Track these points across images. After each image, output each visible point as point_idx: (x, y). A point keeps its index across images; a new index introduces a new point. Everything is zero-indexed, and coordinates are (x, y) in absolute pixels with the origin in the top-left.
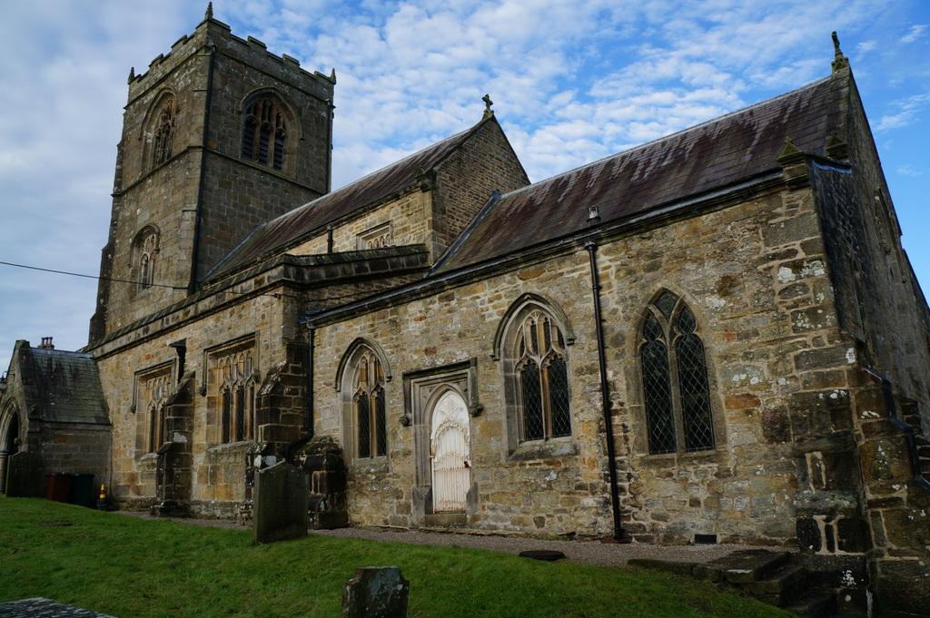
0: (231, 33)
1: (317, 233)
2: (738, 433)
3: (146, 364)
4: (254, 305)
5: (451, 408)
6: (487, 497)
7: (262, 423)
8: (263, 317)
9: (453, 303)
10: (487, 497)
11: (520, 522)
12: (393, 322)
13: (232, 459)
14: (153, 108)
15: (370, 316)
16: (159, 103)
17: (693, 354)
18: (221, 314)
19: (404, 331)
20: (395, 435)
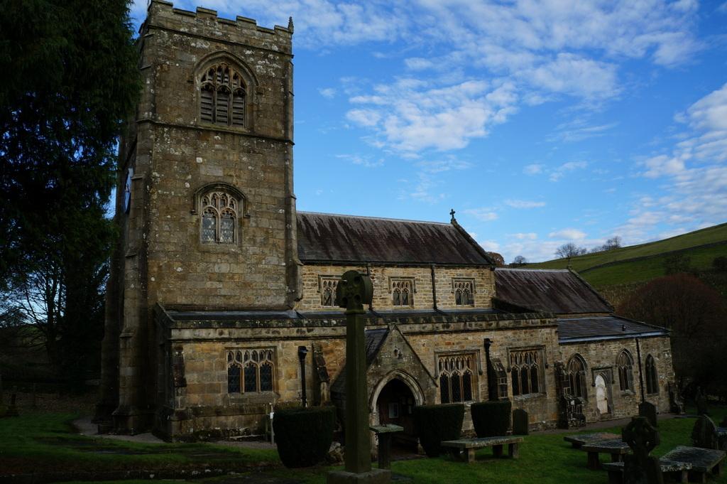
0: (257, 25)
2: (662, 389)
3: (444, 348)
5: (600, 381)
10: (616, 408)
12: (585, 349)
13: (533, 403)
14: (208, 59)
16: (214, 59)
17: (653, 369)
18: (518, 331)
20: (589, 390)
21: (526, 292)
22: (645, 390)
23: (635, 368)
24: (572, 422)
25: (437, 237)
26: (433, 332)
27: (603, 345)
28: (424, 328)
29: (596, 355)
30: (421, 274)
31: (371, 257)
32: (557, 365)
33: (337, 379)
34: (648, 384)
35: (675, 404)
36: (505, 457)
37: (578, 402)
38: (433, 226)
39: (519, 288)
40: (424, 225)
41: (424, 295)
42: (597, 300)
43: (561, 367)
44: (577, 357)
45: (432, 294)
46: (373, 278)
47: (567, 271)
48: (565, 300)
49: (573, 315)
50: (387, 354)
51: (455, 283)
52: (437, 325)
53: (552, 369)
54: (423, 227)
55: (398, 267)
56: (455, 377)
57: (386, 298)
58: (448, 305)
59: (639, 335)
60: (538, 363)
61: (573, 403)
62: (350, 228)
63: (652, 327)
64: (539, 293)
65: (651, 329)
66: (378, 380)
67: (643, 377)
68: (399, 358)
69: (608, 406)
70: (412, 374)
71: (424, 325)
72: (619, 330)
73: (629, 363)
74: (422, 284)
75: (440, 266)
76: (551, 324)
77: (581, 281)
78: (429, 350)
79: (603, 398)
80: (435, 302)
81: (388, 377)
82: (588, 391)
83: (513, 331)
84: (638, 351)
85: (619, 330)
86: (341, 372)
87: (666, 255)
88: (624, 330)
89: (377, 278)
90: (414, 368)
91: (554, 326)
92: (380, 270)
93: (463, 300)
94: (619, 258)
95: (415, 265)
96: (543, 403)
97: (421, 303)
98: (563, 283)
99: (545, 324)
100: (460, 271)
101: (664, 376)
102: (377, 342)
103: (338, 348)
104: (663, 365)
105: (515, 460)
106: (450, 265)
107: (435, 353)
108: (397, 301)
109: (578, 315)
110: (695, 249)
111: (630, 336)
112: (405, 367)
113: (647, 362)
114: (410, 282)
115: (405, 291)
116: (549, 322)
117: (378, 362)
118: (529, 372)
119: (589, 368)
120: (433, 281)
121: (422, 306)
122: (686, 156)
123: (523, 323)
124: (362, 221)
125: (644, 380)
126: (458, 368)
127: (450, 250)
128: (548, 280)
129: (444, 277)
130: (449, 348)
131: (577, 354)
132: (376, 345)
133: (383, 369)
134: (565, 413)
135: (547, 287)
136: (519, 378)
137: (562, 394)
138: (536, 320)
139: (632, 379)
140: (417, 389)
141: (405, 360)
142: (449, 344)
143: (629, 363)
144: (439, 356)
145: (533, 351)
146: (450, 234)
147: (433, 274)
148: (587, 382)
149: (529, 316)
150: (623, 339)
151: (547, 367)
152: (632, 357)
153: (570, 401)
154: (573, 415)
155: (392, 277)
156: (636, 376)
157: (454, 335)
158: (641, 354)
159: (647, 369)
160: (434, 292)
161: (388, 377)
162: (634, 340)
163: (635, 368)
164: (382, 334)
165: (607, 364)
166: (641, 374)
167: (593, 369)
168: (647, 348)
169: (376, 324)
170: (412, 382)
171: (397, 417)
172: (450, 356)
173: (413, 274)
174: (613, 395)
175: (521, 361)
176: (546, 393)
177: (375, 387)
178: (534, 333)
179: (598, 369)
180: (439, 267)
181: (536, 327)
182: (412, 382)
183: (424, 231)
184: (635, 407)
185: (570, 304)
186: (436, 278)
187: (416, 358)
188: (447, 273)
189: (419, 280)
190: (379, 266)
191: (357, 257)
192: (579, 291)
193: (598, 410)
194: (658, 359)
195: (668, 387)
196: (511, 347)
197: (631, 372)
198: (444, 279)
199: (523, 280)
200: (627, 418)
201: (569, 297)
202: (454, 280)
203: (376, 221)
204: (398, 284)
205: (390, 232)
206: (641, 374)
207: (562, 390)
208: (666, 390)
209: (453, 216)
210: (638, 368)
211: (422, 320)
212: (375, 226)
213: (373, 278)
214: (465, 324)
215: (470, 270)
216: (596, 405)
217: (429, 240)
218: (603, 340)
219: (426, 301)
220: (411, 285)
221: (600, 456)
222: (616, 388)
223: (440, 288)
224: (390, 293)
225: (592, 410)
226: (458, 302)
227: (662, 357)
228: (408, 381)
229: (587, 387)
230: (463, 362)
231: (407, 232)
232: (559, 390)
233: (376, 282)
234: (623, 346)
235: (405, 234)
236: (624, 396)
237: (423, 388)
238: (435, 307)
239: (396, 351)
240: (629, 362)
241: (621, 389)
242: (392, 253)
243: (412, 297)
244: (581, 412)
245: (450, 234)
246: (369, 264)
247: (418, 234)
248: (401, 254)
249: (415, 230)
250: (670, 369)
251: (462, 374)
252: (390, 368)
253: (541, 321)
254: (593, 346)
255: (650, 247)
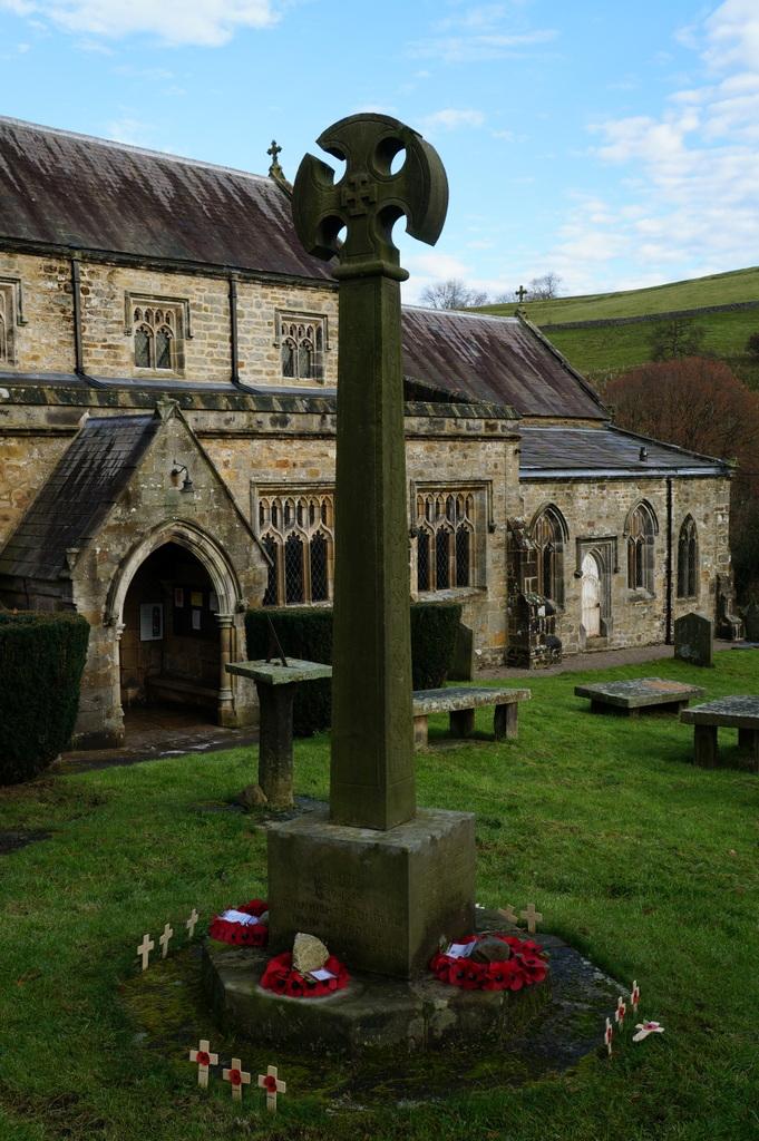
1: (210, 273)
2: (704, 590)
4: (484, 449)
5: (589, 566)
6: (617, 626)
7: (528, 576)
8: (496, 466)
9: (605, 492)
10: (617, 626)
11: (630, 639)
15: (555, 485)
17: (693, 545)
18: (436, 444)
19: (576, 505)
21: (433, 360)
22: (674, 590)
23: (660, 541)
24: (538, 652)
25: (239, 206)
26: (249, 434)
27: (603, 488)
28: (227, 422)
29: (589, 509)
30: (205, 292)
31: (79, 235)
32: (513, 527)
33: (11, 541)
34: (680, 575)
35: (726, 620)
36: (480, 737)
37: (549, 611)
38: (229, 178)
39: (416, 350)
40: (206, 171)
41: (210, 345)
42: (579, 391)
43: (521, 531)
44: (552, 511)
45: (228, 344)
46: (86, 292)
47: (515, 321)
48: (513, 384)
49: (531, 420)
50: (153, 479)
51: (281, 323)
52: (259, 416)
53: (501, 535)
54: (204, 176)
55: (150, 268)
56: (294, 545)
57: (116, 347)
58: (264, 376)
59: (672, 472)
60: (472, 519)
61: (542, 611)
62: (20, 153)
63: (696, 457)
64: (459, 365)
65: (693, 462)
66: (129, 545)
67: (673, 562)
68: (182, 491)
69: (601, 621)
70: (213, 533)
71: (229, 415)
72: (634, 459)
73: (648, 530)
74: (206, 318)
75: (251, 276)
76: (508, 433)
77: (547, 347)
78: (237, 476)
79: (592, 605)
80: (234, 363)
81: (154, 539)
82: (566, 586)
83: (427, 444)
84: (669, 506)
85: (634, 459)
86: (24, 524)
87: (654, 319)
88: (642, 458)
89: (97, 293)
90: (218, 517)
91: (514, 439)
92: (104, 271)
93: (300, 365)
94: (558, 319)
95: (190, 269)
96: (479, 609)
97: (202, 366)
98: (509, 348)
99: (495, 433)
100: (295, 295)
101: (713, 561)
102: (122, 449)
103: (14, 462)
104: (712, 538)
105: (511, 742)
106: (275, 278)
107: (253, 484)
108: (144, 357)
109: (540, 420)
110: (714, 313)
111: (655, 473)
112: (195, 517)
113: (683, 531)
114: (178, 310)
115: (164, 332)
116: (503, 427)
117: (130, 500)
118: (453, 540)
119: (573, 536)
120: (232, 312)
121: (202, 374)
122: (690, 123)
123: (449, 426)
124: (50, 141)
125: (674, 568)
126: (300, 523)
127: (271, 241)
128: (478, 338)
129: (259, 306)
130: (284, 475)
131: (552, 506)
132: (122, 455)
133: (142, 518)
134: (525, 635)
135: (476, 354)
136: (432, 551)
137: (519, 591)
138: (477, 422)
139: (651, 565)
140: (223, 570)
141: (197, 498)
142: (284, 464)
143: (648, 530)
144: (262, 493)
145: (465, 494)
146: (268, 201)
147: (232, 296)
148: (565, 568)
149: (462, 411)
150: (638, 476)
151: (492, 530)
152: (655, 518)
153: (537, 607)
154: (542, 636)
155: (133, 295)
156: (659, 560)
157: (297, 444)
158: (673, 513)
159: (681, 544)
160: (233, 340)
161: (154, 539)
162: (664, 482)
163: (660, 541)
164: (140, 430)
165: (608, 531)
166: (669, 554)
167: (578, 540)
168: (686, 501)
169: (114, 406)
170: (212, 551)
171: (161, 637)
172: (286, 493)
173: (186, 291)
174: (614, 598)
175: (438, 513)
176: (485, 589)
177: (123, 563)
178: (468, 452)
179: (590, 540)
180: (246, 280)
181: (475, 438)
182: (212, 551)
183: (206, 185)
184: (652, 624)
185: (524, 394)
186: (239, 307)
187: (225, 493)
188: (265, 296)
189: (198, 307)
190: (103, 263)
191: (44, 233)
192: (540, 366)
193: (582, 629)
194: (704, 526)
195: (717, 586)
196: (420, 479)
197: (651, 550)
198: (258, 312)
199: (424, 331)
200: (635, 646)
201: (521, 379)
202: (281, 315)
203: (87, 145)
204: (148, 314)
205: (125, 180)
206: (669, 554)
207: (519, 580)
208: (711, 591)
209: (275, 159)
210: (665, 542)
211: (225, 401)
212: (86, 159)
213: (86, 292)
214: (324, 418)
215: (317, 296)
216: (580, 618)
217: (219, 210)
218: (604, 478)
219: (215, 362)
220: (180, 319)
221: (719, 733)
222: (620, 583)
223: (248, 332)
224: (128, 333)
225: (570, 629)
226: (288, 370)
227: (711, 520)
228: (202, 549)
229: (566, 578)
230: (312, 509)
231: (166, 182)
232: (513, 583)
233: (95, 302)
234: (641, 494)
235: (162, 187)
236: (633, 600)
237: (237, 567)
238: (234, 379)
239: (175, 473)
240: (649, 529)
241: (630, 587)
242: (132, 232)
243: (180, 348)
244: (553, 632)
245: (268, 201)
246: (77, 255)
247: (194, 193)
248: (154, 237)
249: (187, 184)
250: (724, 548)
251: (310, 538)
252: (160, 516)
253: (487, 425)
254: (582, 488)
255: (620, 300)
